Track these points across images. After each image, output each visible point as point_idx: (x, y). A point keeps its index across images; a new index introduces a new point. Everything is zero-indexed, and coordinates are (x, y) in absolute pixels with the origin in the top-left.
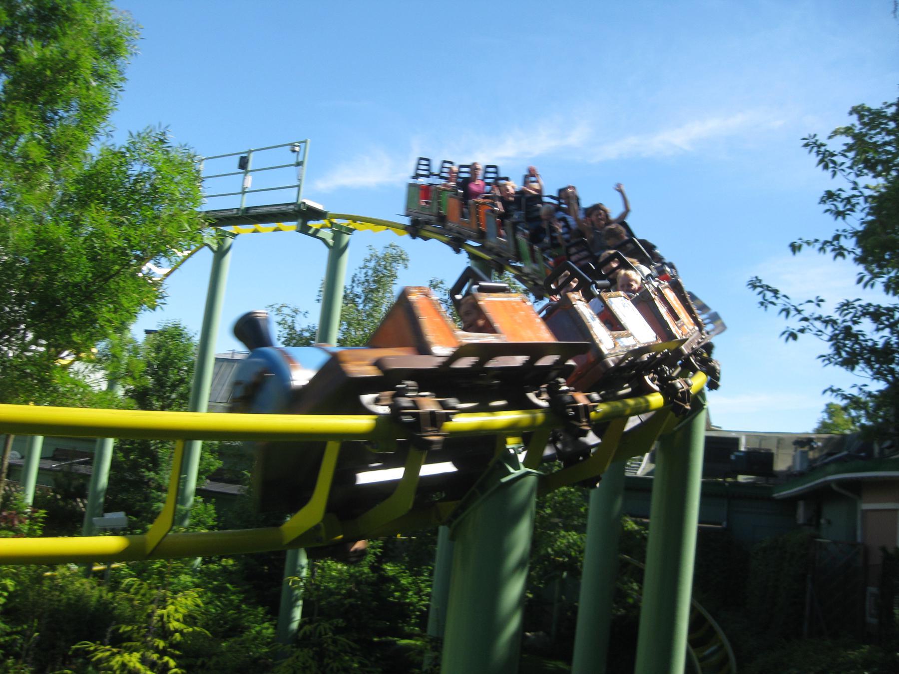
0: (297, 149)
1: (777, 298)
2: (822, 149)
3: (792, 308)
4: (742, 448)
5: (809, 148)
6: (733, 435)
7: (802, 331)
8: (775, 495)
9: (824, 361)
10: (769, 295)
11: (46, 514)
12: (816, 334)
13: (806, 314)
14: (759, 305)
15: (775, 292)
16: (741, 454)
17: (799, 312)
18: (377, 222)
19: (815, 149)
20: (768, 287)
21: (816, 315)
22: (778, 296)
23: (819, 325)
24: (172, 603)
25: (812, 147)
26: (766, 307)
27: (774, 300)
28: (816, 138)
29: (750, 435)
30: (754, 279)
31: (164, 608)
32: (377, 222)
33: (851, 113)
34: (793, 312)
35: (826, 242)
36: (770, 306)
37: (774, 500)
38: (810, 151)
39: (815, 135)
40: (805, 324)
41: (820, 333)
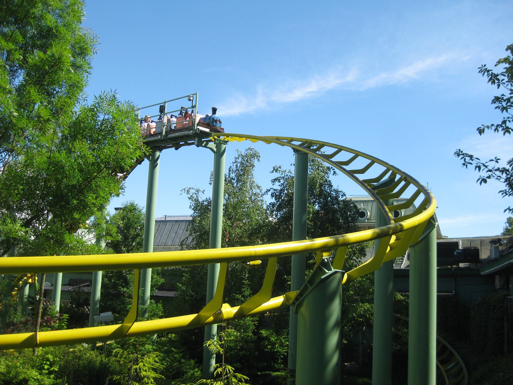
0: (192, 98)
1: (472, 160)
2: (490, 72)
3: (481, 165)
4: (460, 248)
5: (483, 73)
6: (455, 240)
7: (489, 177)
8: (481, 273)
9: (502, 194)
10: (468, 159)
11: (68, 316)
12: (498, 179)
13: (490, 168)
14: (463, 165)
15: (471, 157)
16: (460, 251)
17: (486, 167)
18: (240, 136)
19: (486, 74)
20: (466, 154)
21: (496, 168)
22: (473, 159)
23: (498, 173)
24: (142, 362)
25: (485, 72)
26: (467, 166)
27: (470, 161)
28: (486, 67)
29: (464, 240)
30: (458, 151)
31: (137, 364)
32: (240, 136)
33: (507, 50)
34: (482, 167)
35: (498, 126)
36: (469, 165)
37: (481, 276)
38: (483, 75)
39: (485, 65)
40: (490, 173)
41: (499, 178)
